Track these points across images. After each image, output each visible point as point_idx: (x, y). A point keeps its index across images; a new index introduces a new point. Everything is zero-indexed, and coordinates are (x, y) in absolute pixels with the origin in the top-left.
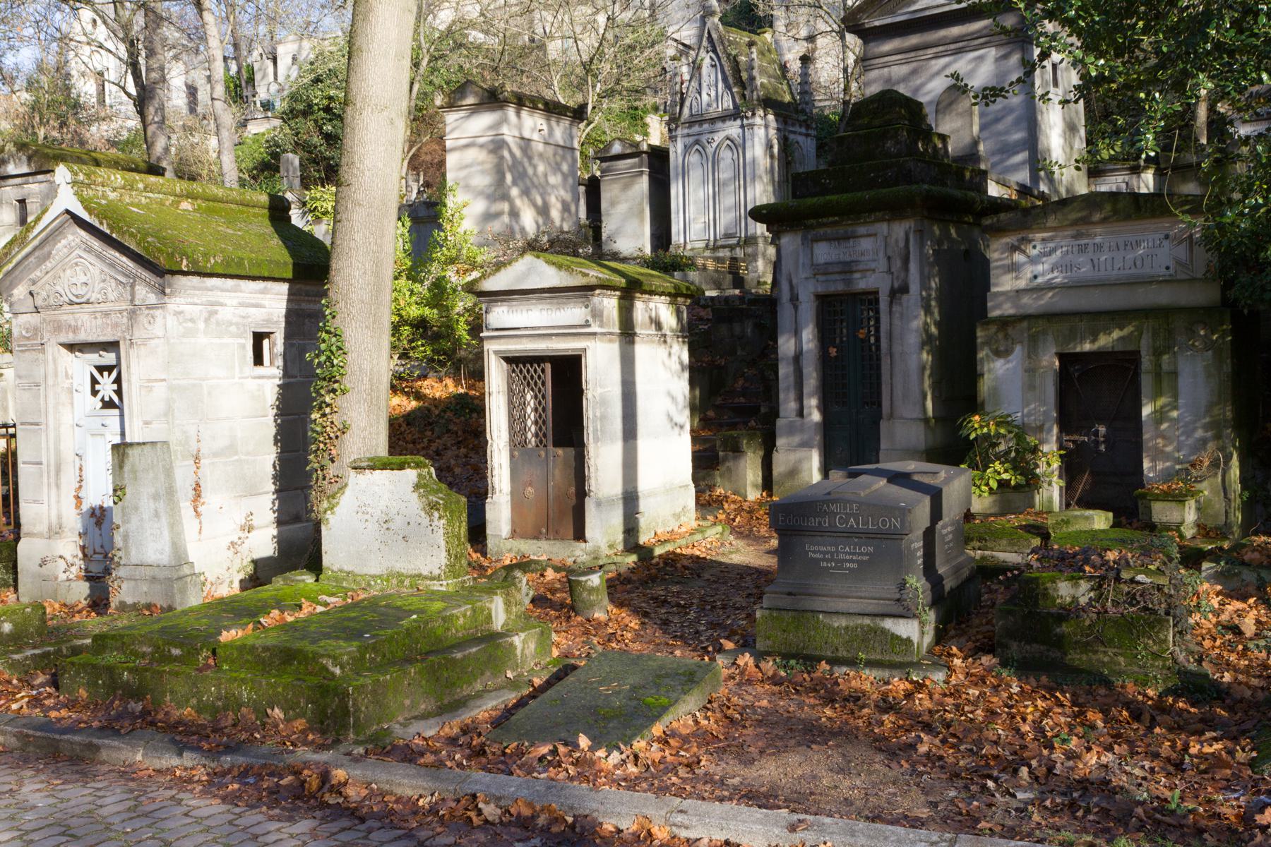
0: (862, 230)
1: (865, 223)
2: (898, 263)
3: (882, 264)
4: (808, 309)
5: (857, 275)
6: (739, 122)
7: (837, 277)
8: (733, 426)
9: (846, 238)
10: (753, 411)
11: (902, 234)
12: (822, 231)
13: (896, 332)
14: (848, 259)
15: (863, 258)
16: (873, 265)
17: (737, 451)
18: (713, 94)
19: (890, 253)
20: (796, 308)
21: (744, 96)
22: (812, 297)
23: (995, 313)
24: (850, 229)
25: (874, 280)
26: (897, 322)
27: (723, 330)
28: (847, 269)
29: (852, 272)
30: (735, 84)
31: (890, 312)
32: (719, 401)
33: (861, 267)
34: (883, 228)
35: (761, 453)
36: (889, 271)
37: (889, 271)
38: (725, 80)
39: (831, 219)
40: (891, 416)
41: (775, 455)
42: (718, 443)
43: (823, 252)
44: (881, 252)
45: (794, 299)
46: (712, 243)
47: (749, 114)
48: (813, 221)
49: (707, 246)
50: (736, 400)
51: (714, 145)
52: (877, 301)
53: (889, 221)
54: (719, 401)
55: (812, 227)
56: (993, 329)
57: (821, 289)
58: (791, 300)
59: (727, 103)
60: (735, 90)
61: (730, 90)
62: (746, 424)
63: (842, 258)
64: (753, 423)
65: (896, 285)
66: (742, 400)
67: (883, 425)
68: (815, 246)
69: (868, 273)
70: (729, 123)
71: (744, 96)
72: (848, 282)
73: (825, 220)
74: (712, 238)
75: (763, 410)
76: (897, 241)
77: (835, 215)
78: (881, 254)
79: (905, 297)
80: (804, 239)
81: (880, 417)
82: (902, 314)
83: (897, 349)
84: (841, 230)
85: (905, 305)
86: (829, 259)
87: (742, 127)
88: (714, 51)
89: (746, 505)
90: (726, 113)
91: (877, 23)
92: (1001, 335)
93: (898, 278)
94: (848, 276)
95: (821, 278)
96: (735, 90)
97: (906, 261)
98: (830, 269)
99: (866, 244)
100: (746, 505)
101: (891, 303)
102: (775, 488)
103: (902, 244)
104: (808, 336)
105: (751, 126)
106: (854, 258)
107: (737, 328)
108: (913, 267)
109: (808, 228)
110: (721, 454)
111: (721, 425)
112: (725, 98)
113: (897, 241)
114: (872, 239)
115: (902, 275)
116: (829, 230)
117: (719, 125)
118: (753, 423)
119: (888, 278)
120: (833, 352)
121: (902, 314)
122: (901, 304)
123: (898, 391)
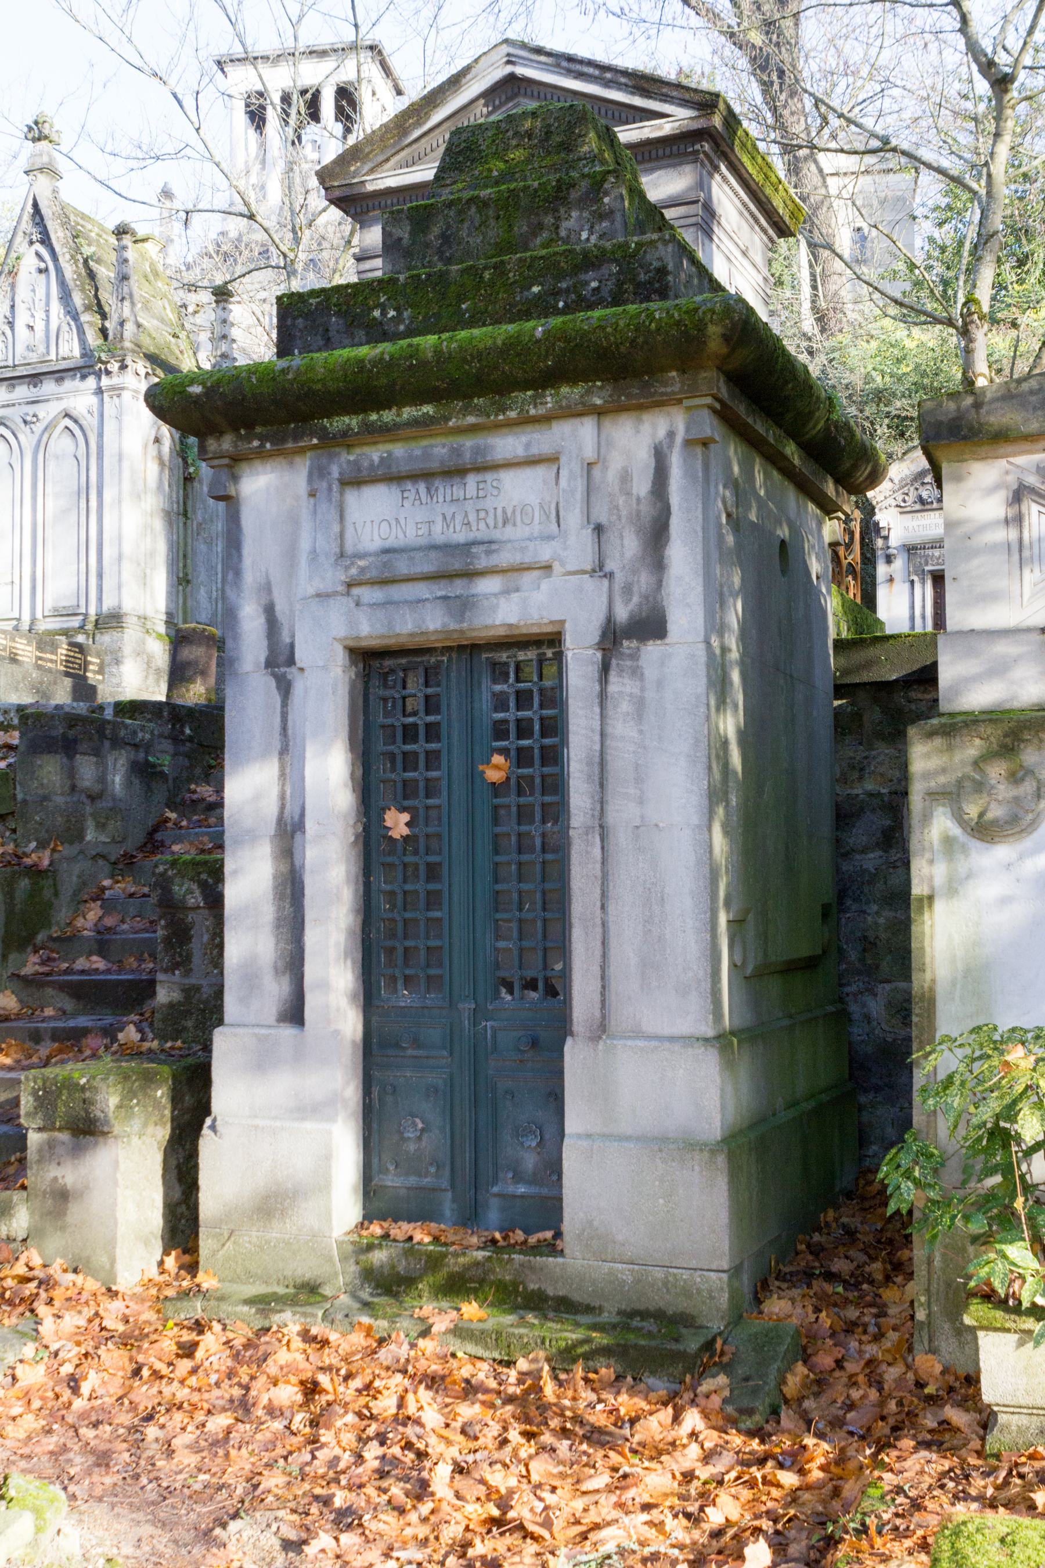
0: (508, 445)
1: (526, 421)
2: (627, 546)
3: (576, 548)
4: (326, 689)
5: (487, 586)
6: (91, 382)
7: (422, 590)
8: (70, 1041)
9: (455, 472)
10: (135, 995)
11: (643, 457)
12: (375, 454)
13: (621, 761)
14: (460, 536)
15: (509, 532)
16: (545, 553)
17: (86, 1129)
18: (40, 326)
19: (601, 515)
20: (285, 688)
21: (104, 332)
22: (341, 657)
23: (980, 697)
24: (468, 443)
25: (551, 594)
26: (621, 728)
27: (50, 771)
28: (456, 566)
29: (471, 574)
30: (88, 308)
31: (603, 696)
32: (32, 965)
33: (505, 558)
34: (579, 436)
35: (163, 1133)
36: (599, 570)
37: (599, 570)
38: (66, 297)
39: (408, 412)
40: (601, 1029)
41: (208, 1145)
42: (26, 1103)
43: (381, 517)
44: (568, 517)
45: (281, 660)
46: (25, 626)
47: (114, 367)
48: (353, 422)
49: (16, 629)
50: (81, 963)
51: (38, 428)
52: (404, 736)
53: (600, 413)
54: (32, 965)
55: (345, 440)
56: (972, 748)
57: (369, 629)
58: (270, 663)
59: (70, 349)
60: (85, 318)
61: (75, 317)
62: (110, 1033)
63: (440, 533)
64: (130, 1034)
65: (622, 614)
66: (98, 963)
67: (576, 1056)
68: (352, 497)
69: (527, 579)
70: (69, 384)
71: (104, 332)
72: (464, 605)
73: (388, 416)
74: (26, 618)
75: (164, 995)
76: (625, 477)
77: (419, 397)
78: (573, 518)
79: (652, 650)
80: (318, 473)
81: (562, 1027)
82: (640, 705)
83: (623, 813)
84: (439, 449)
85: (650, 673)
86: (395, 538)
87: (99, 391)
88: (46, 240)
89: (112, 1314)
90: (64, 365)
91: (392, 182)
92: (996, 771)
93: (628, 590)
94: (458, 587)
95: (369, 594)
96: (85, 318)
97: (657, 535)
98: (403, 567)
99: (519, 489)
100: (112, 1314)
101: (605, 669)
102: (206, 1244)
103: (642, 486)
104: (330, 772)
105: (117, 390)
106: (480, 532)
107: (87, 770)
108: (683, 555)
109: (332, 442)
110: (34, 1138)
111: (36, 1037)
112: (65, 335)
113: (625, 477)
114: (541, 472)
115: (644, 580)
116: (399, 450)
117: (49, 387)
118: (130, 1034)
119: (596, 592)
120: (398, 823)
121: (640, 705)
122: (636, 673)
123: (626, 951)
